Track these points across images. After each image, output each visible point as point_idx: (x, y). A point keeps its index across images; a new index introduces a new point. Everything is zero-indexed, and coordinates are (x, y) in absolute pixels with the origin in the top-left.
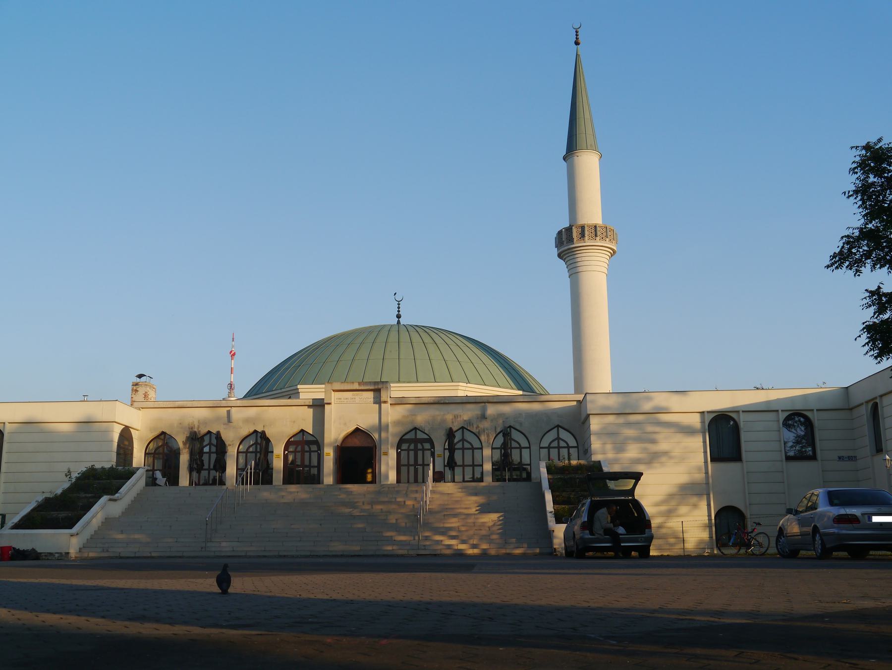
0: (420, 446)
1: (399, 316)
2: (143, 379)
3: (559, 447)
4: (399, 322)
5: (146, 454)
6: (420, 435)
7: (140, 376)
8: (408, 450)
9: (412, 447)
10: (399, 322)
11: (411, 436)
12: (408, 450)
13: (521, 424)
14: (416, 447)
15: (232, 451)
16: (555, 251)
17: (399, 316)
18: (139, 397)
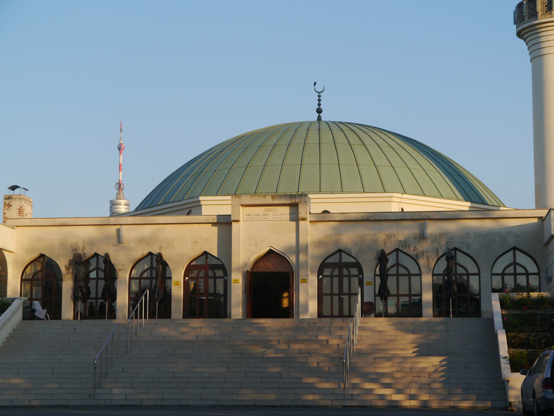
0: (345, 272)
1: (319, 111)
2: (17, 191)
3: (515, 274)
4: (319, 118)
5: (22, 280)
6: (346, 259)
7: (13, 188)
8: (332, 276)
9: (336, 272)
10: (319, 118)
11: (201, 262)
12: (332, 276)
13: (468, 245)
14: (341, 272)
15: (123, 276)
16: (514, 29)
17: (319, 111)
18: (13, 213)
